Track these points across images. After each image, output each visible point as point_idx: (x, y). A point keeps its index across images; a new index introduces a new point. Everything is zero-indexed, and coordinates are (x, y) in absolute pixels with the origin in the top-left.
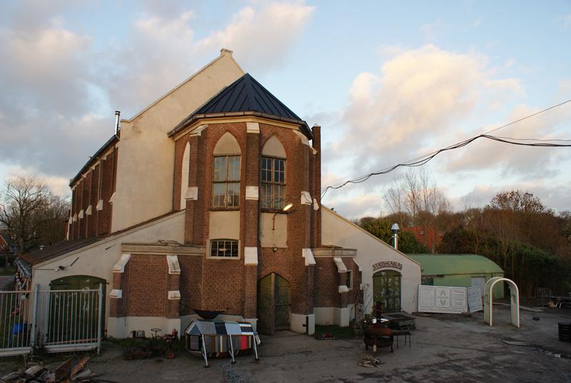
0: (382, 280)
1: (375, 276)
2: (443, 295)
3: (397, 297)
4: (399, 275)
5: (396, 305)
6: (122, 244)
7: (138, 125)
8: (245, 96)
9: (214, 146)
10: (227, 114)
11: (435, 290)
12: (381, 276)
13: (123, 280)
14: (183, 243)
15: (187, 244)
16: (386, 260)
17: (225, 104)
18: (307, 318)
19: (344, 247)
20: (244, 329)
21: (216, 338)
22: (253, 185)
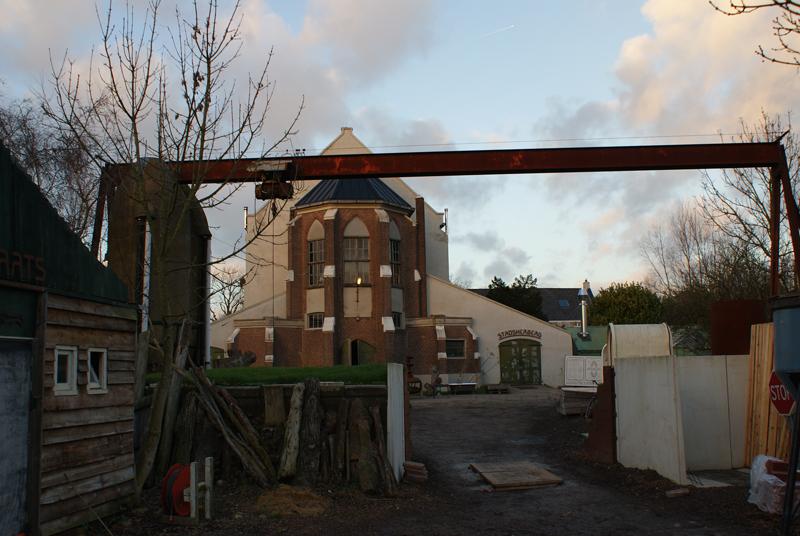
1: (501, 346)
4: (538, 345)
5: (534, 377)
9: (307, 233)
11: (585, 361)
15: (289, 318)
16: (516, 329)
19: (447, 315)
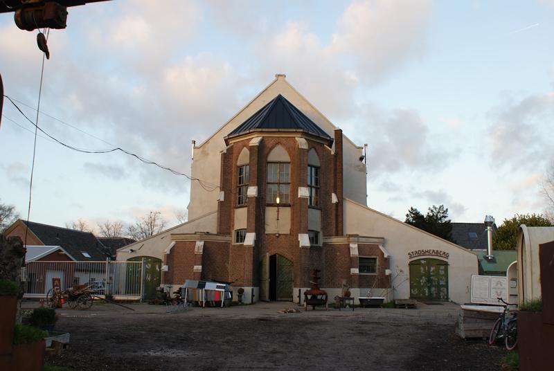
0: (422, 268)
1: (411, 264)
2: (499, 285)
3: (443, 286)
4: (446, 264)
6: (172, 234)
7: (206, 149)
8: (279, 115)
9: (237, 159)
10: (264, 130)
11: (490, 281)
12: (420, 264)
13: (170, 257)
14: (216, 233)
17: (70, 147)
18: (300, 290)
19: (360, 235)
20: (218, 287)
21: (197, 291)
22: (253, 186)
